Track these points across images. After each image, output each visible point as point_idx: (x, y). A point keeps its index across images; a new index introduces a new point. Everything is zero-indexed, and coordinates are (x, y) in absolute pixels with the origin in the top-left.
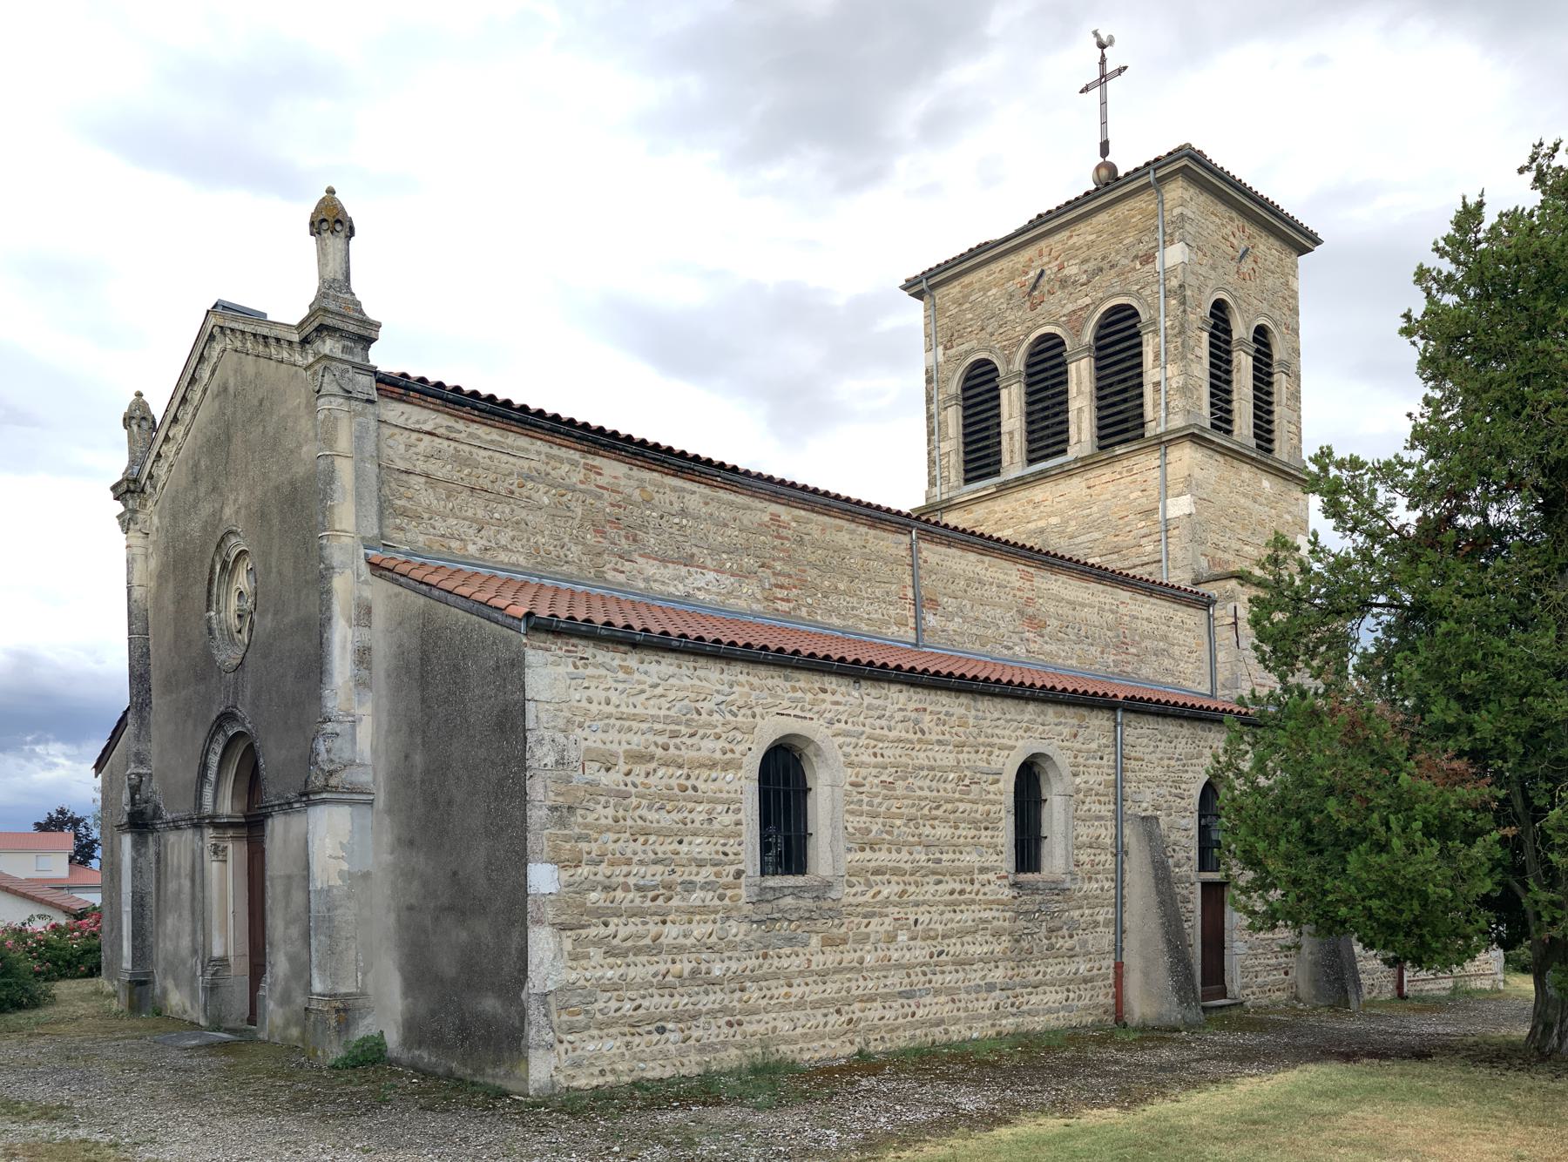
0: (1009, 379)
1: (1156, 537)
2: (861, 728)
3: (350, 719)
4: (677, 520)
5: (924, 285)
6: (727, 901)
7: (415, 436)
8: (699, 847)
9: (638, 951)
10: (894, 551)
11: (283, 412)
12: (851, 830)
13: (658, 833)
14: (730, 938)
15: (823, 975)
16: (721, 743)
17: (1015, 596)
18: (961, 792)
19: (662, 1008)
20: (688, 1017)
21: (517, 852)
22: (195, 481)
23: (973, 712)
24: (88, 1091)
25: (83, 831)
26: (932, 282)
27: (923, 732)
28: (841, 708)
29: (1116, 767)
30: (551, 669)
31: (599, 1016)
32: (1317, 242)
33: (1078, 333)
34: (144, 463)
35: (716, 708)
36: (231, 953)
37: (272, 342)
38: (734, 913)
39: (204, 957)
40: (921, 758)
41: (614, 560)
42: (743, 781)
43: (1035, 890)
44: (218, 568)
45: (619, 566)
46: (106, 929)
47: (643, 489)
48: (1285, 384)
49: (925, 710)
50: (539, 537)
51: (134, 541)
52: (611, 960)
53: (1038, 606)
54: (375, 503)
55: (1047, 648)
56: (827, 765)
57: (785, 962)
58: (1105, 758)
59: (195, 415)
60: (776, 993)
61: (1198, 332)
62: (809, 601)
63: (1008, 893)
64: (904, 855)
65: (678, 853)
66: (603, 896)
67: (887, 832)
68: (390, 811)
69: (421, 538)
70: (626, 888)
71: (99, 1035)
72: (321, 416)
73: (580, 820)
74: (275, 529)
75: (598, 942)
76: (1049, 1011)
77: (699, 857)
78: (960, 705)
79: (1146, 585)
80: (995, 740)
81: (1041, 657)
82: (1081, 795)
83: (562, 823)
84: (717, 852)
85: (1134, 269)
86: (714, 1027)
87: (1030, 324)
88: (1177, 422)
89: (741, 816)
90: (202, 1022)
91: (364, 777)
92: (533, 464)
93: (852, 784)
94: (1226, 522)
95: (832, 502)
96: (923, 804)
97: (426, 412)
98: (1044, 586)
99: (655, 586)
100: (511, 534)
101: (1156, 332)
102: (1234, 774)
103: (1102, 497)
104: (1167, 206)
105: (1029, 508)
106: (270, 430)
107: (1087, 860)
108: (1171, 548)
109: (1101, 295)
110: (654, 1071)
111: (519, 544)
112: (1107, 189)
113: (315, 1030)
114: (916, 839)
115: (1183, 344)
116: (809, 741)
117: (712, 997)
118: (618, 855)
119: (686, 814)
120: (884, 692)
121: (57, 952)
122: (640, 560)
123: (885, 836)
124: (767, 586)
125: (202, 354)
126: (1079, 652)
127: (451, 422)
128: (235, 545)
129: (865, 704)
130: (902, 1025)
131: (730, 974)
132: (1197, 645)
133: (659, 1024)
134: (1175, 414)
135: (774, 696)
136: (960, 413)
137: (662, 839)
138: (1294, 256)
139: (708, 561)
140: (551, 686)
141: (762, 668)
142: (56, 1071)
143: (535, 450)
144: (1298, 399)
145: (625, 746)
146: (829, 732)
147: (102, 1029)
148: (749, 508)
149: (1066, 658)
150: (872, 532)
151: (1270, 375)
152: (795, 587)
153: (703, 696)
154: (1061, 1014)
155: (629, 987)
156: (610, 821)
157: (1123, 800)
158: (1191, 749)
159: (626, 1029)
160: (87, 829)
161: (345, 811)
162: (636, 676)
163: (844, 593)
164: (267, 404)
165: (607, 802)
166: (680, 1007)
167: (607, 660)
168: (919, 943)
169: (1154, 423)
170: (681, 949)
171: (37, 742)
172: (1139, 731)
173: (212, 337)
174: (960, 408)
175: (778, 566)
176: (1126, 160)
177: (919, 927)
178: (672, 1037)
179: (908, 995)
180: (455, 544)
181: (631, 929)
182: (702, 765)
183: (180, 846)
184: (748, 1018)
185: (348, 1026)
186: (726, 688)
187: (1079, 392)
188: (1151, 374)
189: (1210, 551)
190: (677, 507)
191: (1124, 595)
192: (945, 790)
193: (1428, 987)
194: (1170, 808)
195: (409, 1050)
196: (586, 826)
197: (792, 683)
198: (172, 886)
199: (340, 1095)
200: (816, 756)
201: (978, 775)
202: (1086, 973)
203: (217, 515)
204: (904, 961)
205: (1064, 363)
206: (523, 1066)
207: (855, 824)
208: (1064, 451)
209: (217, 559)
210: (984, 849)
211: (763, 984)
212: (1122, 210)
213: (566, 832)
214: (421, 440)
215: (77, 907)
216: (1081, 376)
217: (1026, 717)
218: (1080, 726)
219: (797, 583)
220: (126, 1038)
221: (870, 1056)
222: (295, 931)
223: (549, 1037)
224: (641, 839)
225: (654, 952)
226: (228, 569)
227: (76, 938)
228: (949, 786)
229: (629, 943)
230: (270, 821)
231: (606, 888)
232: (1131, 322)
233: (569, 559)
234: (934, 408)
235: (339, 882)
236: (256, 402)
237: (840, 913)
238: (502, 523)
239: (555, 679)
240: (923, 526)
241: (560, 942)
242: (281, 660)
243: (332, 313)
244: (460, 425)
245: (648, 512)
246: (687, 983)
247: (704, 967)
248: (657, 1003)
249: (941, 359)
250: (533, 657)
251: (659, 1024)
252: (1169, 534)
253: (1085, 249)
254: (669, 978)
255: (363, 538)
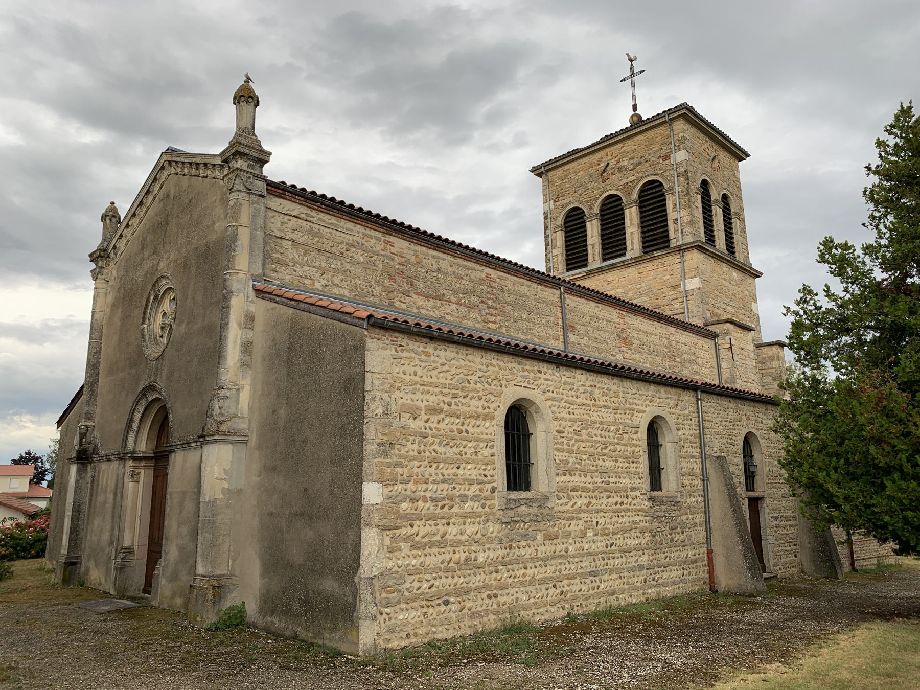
0: (591, 217)
1: (681, 300)
3: (236, 387)
4: (435, 275)
5: (543, 170)
6: (487, 509)
7: (287, 217)
8: (470, 471)
9: (432, 545)
11: (204, 205)
13: (445, 461)
14: (489, 534)
15: (545, 560)
16: (482, 403)
18: (618, 438)
19: (447, 587)
20: (462, 592)
21: (355, 475)
22: (143, 248)
23: (622, 389)
24: (31, 652)
25: (40, 464)
26: (547, 168)
27: (595, 400)
28: (550, 383)
29: (699, 426)
30: (382, 352)
31: (406, 594)
32: (748, 156)
33: (629, 194)
34: (112, 240)
35: (479, 380)
36: (136, 544)
37: (202, 166)
38: (491, 517)
39: (117, 546)
40: (595, 417)
41: (400, 296)
42: (495, 427)
43: (662, 503)
44: (152, 298)
45: (402, 299)
46: (52, 526)
47: (417, 256)
48: (738, 224)
49: (595, 386)
50: (357, 280)
51: (99, 285)
52: (415, 552)
53: (628, 333)
54: (261, 254)
57: (522, 552)
59: (146, 212)
60: (517, 573)
63: (647, 504)
64: (589, 479)
65: (457, 475)
66: (411, 505)
68: (259, 447)
69: (288, 277)
70: (425, 501)
71: (41, 602)
72: (231, 203)
73: (397, 452)
74: (193, 272)
75: (407, 539)
76: (674, 583)
77: (470, 478)
78: (615, 384)
83: (386, 454)
84: (480, 475)
85: (659, 163)
86: (480, 599)
87: (602, 189)
88: (689, 239)
89: (494, 450)
90: (112, 592)
91: (242, 425)
92: (355, 238)
93: (558, 432)
94: (718, 293)
95: (519, 269)
96: (597, 445)
97: (294, 204)
99: (423, 312)
100: (341, 277)
101: (673, 194)
104: (675, 133)
106: (195, 216)
108: (690, 306)
109: (641, 175)
110: (442, 634)
111: (346, 283)
113: (197, 601)
115: (689, 200)
116: (532, 403)
117: (478, 577)
118: (420, 476)
119: (461, 449)
120: (573, 374)
121: (18, 541)
122: (414, 296)
123: (577, 466)
125: (156, 177)
126: (651, 360)
127: (309, 211)
128: (164, 284)
130: (592, 595)
131: (489, 560)
132: (710, 358)
133: (445, 598)
135: (512, 374)
136: (564, 235)
137: (447, 465)
139: (452, 298)
140: (382, 362)
141: (506, 356)
142: (8, 633)
143: (356, 231)
144: (745, 232)
145: (425, 403)
146: (544, 398)
147: (43, 597)
148: (474, 269)
150: (540, 287)
153: (471, 372)
154: (681, 585)
155: (426, 571)
156: (416, 453)
157: (705, 446)
158: (736, 416)
159: (424, 603)
160: (42, 463)
161: (229, 447)
162: (433, 358)
163: (525, 320)
164: (194, 201)
165: (414, 440)
166: (458, 586)
167: (416, 347)
168: (599, 538)
170: (458, 543)
171: (15, 414)
172: (709, 404)
173: (163, 168)
175: (490, 303)
176: (646, 113)
177: (599, 527)
178: (453, 607)
179: (594, 574)
180: (307, 282)
181: (428, 528)
182: (471, 417)
183: (108, 472)
184: (501, 592)
185: (220, 599)
186: (484, 368)
187: (631, 224)
188: (671, 215)
189: (711, 308)
190: (435, 267)
191: (672, 330)
192: (609, 437)
193: (866, 563)
194: (728, 451)
195: (264, 617)
196: (400, 456)
198: (100, 498)
199: (218, 655)
200: (536, 412)
201: (627, 428)
202: (692, 557)
203: (155, 268)
204: (591, 551)
205: (622, 209)
206: (354, 633)
207: (560, 457)
208: (624, 254)
209: (152, 293)
210: (633, 476)
211: (510, 567)
213: (388, 460)
214: (290, 220)
215: (31, 510)
216: (632, 217)
217: (650, 393)
220: (58, 604)
221: (576, 617)
222: (185, 530)
223: (374, 611)
224: (435, 466)
225: (442, 545)
226: (158, 300)
227: (31, 532)
228: (611, 434)
229: (426, 539)
230: (173, 455)
231: (413, 500)
233: (374, 294)
234: (549, 232)
235: (222, 496)
236: (188, 202)
237: (554, 517)
238: (336, 271)
239: (384, 358)
240: (567, 285)
241: (382, 540)
242: (189, 352)
243: (243, 145)
244: (314, 213)
245: (419, 269)
246: (463, 567)
247: (473, 555)
248: (444, 582)
249: (552, 207)
250: (370, 344)
251: (445, 598)
252: (688, 298)
254: (451, 564)
255: (252, 275)
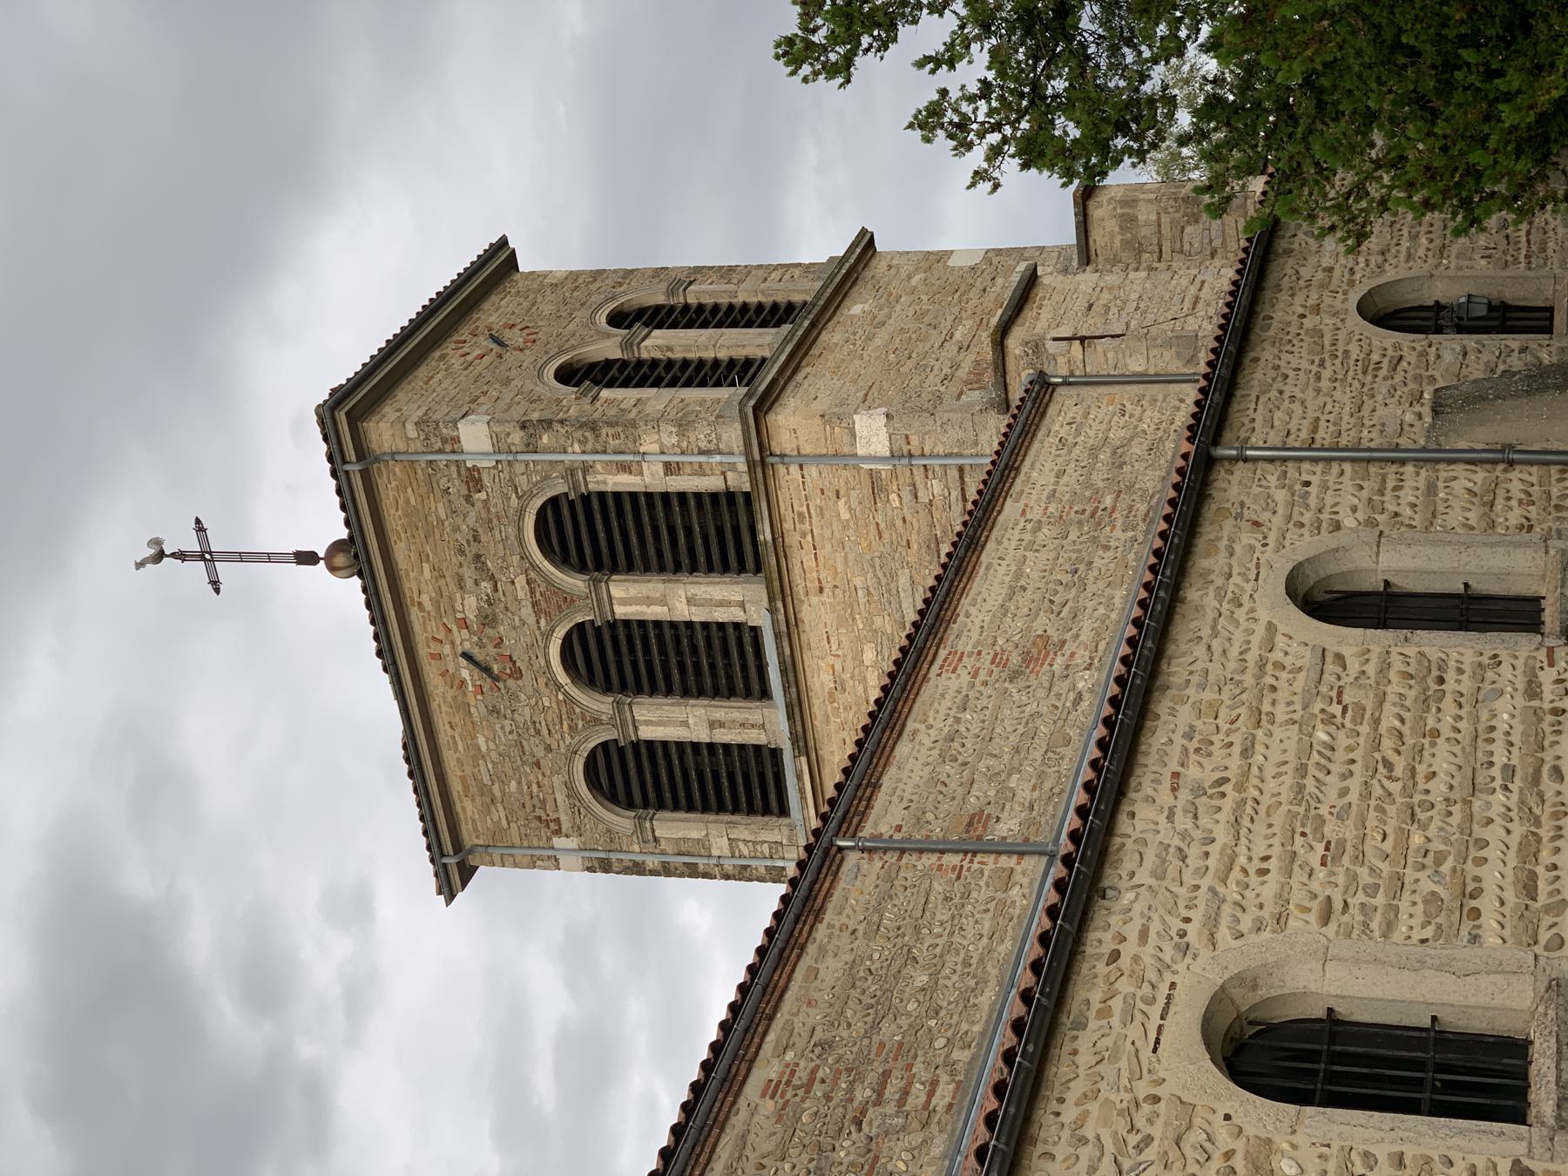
0: (623, 723)
1: (919, 475)
2: (1203, 893)
5: (451, 861)
10: (870, 882)
12: (1429, 932)
17: (985, 683)
23: (1191, 691)
26: (448, 847)
27: (1224, 781)
28: (1155, 927)
29: (1329, 460)
32: (503, 242)
33: (568, 600)
40: (1279, 787)
42: (1298, 1139)
48: (705, 287)
49: (1176, 775)
53: (1011, 645)
55: (1086, 635)
56: (1277, 965)
58: (1305, 477)
61: (598, 404)
62: (939, 1043)
64: (1494, 833)
67: (1439, 862)
78: (1173, 712)
79: (996, 476)
80: (1252, 657)
81: (1102, 646)
82: (1380, 518)
85: (486, 502)
87: (542, 681)
88: (732, 435)
89: (1381, 1153)
93: (1326, 919)
94: (910, 364)
95: (761, 980)
96: (1377, 791)
98: (975, 635)
101: (587, 468)
102: (1359, 199)
103: (840, 568)
104: (402, 447)
105: (842, 699)
107: (1518, 511)
108: (940, 449)
109: (516, 559)
112: (362, 556)
114: (1456, 809)
116: (1220, 998)
120: (1130, 844)
123: (1446, 868)
124: (900, 1121)
126: (1101, 584)
129: (1152, 882)
132: (1111, 403)
134: (719, 439)
135: (1115, 1054)
138: (516, 277)
141: (1051, 1071)
144: (731, 269)
146: (1205, 954)
148: (743, 1137)
149: (1110, 606)
150: (829, 916)
151: (686, 307)
152: (909, 1067)
163: (934, 976)
169: (730, 475)
172: (1258, 425)
174: (660, 814)
175: (863, 1093)
186: (1087, 1152)
187: (662, 601)
188: (651, 479)
189: (954, 388)
191: (1010, 510)
192: (1350, 749)
194: (1418, 378)
197: (1092, 1015)
200: (1255, 987)
201: (1324, 689)
205: (613, 625)
207: (1416, 922)
208: (755, 630)
210: (1487, 686)
212: (394, 520)
217: (1210, 602)
218: (1239, 516)
219: (901, 1063)
228: (1343, 740)
232: (566, 512)
234: (652, 862)
240: (833, 825)
249: (573, 843)
253: (442, 582)
